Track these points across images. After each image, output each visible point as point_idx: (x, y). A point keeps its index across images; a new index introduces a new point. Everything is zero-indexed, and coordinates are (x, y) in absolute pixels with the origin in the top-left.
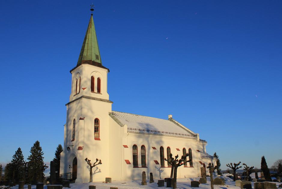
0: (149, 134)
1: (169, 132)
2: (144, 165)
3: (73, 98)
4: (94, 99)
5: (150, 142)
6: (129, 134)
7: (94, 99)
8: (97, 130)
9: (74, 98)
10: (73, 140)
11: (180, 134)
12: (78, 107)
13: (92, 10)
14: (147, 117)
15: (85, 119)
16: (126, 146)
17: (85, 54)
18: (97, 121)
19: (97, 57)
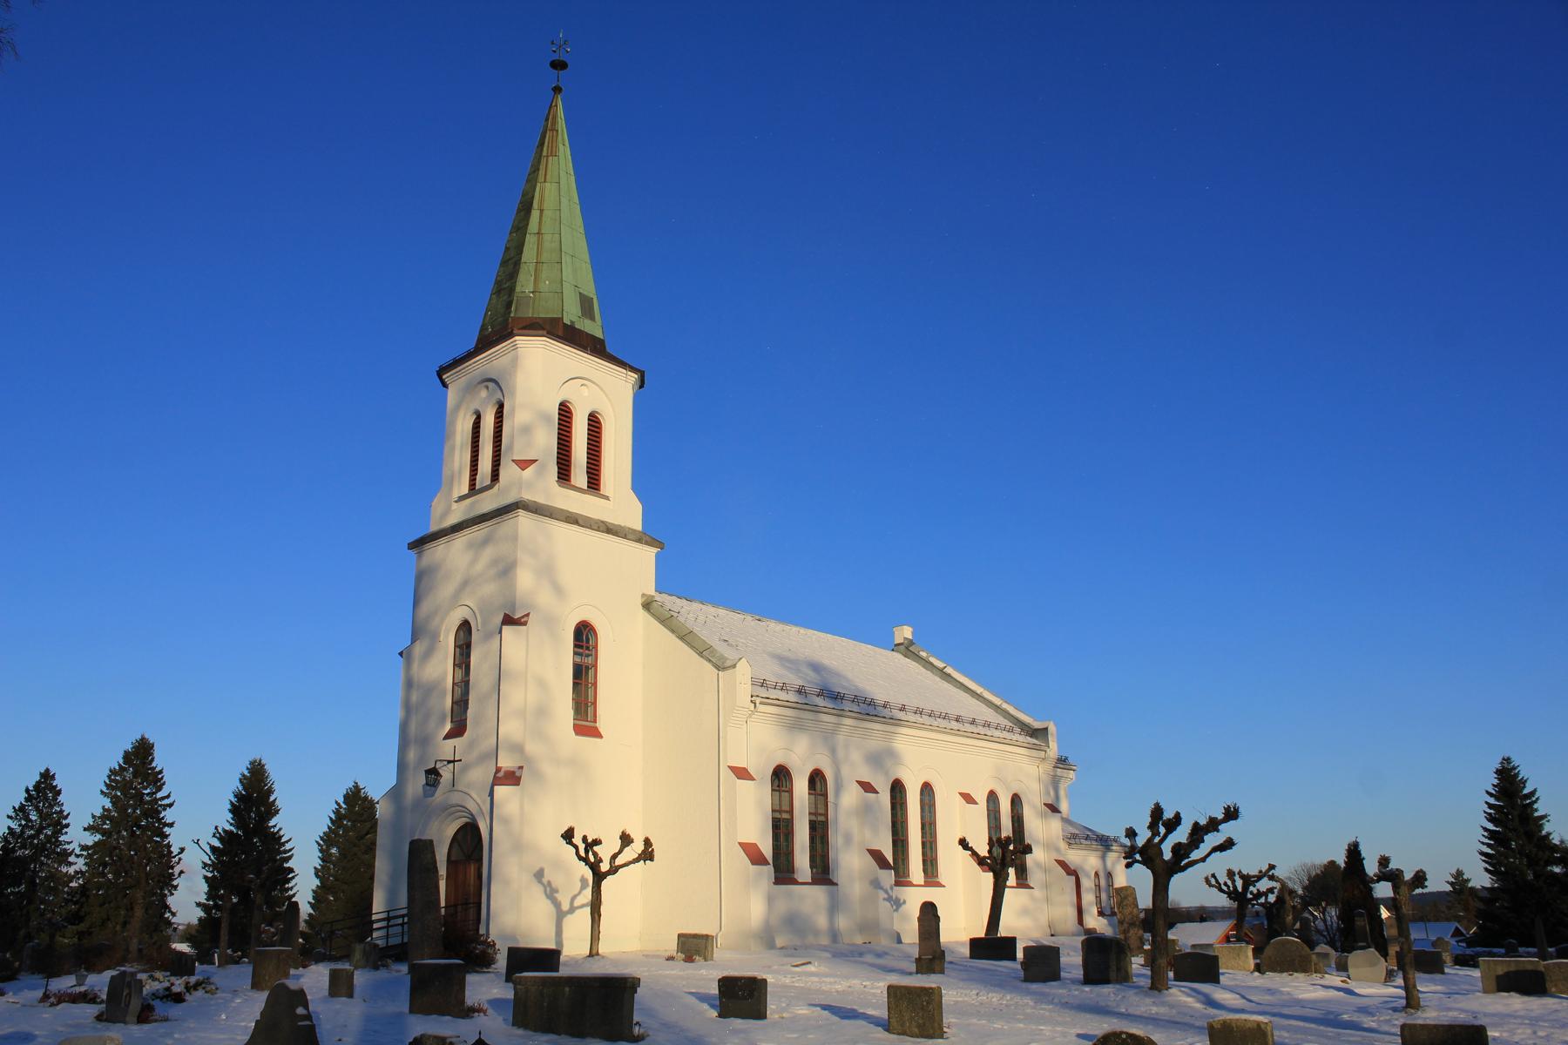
0: (840, 714)
1: (928, 707)
2: (823, 873)
3: (447, 512)
4: (573, 519)
5: (841, 753)
6: (761, 708)
7: (573, 519)
8: (583, 676)
9: (457, 514)
10: (458, 730)
11: (973, 722)
12: (480, 566)
13: (559, 65)
14: (802, 631)
15: (531, 619)
16: (742, 773)
17: (525, 284)
18: (584, 635)
19: (586, 306)
